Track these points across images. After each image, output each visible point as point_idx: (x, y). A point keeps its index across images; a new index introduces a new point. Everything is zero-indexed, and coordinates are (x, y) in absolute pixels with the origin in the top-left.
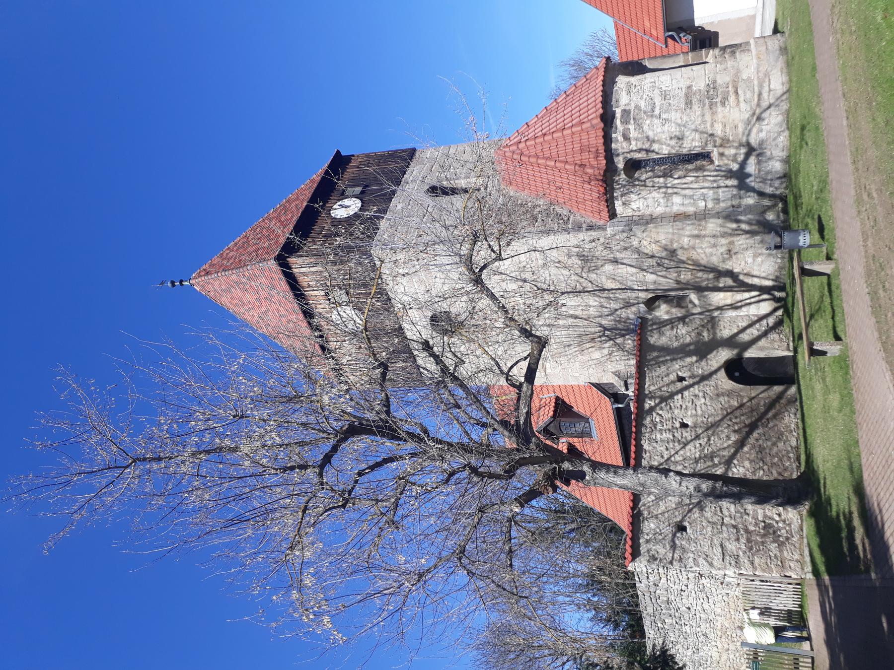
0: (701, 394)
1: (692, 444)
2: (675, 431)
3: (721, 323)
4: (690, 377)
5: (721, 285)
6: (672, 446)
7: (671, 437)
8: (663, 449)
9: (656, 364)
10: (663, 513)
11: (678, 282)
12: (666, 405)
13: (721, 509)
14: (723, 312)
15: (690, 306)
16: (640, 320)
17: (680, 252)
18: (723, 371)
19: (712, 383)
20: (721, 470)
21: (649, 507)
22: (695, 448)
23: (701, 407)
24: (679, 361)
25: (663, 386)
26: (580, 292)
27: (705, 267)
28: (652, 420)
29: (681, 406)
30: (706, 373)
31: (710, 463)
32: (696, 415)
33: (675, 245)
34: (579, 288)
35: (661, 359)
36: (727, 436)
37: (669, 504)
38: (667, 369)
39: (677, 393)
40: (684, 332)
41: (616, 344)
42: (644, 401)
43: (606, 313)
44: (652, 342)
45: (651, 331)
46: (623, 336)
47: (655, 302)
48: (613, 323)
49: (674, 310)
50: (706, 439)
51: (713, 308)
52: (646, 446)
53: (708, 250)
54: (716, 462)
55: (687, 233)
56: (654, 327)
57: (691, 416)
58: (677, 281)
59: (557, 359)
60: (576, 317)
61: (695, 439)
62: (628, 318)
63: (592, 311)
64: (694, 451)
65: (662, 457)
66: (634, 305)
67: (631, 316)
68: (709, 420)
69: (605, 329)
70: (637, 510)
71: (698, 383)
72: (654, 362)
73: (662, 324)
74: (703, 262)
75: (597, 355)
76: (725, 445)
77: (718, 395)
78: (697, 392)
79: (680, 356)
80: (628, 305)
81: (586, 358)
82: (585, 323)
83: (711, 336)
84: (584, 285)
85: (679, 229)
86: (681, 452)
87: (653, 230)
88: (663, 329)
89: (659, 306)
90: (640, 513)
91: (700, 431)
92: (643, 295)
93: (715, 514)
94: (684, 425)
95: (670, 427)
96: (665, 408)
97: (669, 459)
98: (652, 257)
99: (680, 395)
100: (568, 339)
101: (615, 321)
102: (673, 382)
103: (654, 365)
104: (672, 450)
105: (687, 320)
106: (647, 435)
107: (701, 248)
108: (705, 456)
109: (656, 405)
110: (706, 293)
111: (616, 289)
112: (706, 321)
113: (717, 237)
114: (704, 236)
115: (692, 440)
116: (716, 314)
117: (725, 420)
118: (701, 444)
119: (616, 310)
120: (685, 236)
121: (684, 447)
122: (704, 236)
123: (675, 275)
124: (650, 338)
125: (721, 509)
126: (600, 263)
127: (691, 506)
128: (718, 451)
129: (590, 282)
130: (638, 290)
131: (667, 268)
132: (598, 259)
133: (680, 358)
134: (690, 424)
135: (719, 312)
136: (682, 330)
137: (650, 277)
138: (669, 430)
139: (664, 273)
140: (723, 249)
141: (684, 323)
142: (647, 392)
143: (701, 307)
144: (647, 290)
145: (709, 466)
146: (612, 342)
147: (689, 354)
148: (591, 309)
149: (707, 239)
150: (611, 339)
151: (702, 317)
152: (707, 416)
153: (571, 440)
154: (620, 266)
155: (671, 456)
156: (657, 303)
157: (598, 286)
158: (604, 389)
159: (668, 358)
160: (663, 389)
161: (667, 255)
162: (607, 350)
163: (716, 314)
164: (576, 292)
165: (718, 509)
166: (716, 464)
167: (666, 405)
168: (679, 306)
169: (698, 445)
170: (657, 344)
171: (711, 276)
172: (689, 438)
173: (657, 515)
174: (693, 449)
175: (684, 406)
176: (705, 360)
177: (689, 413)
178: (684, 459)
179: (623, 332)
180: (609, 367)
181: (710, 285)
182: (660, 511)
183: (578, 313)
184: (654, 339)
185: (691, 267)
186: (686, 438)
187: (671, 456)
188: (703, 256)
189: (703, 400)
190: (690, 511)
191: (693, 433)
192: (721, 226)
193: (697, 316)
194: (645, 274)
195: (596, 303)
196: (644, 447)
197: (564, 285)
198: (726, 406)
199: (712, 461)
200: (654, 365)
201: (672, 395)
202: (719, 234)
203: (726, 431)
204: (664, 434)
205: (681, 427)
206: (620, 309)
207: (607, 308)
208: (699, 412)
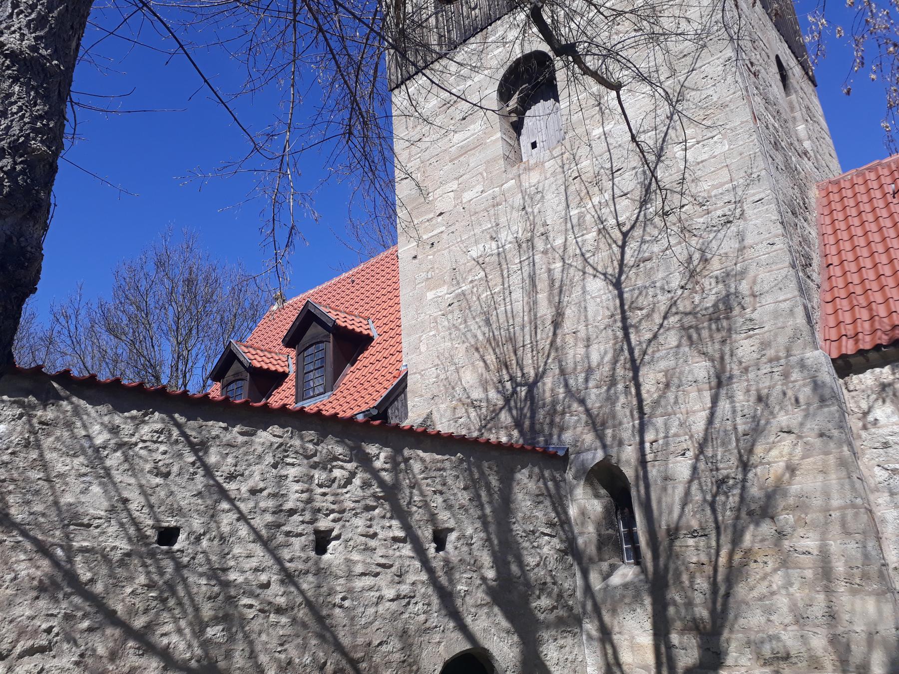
0: (405, 589)
1: (269, 561)
2: (308, 516)
3: (569, 641)
4: (447, 561)
5: (675, 638)
6: (263, 504)
7: (289, 505)
8: (255, 481)
9: (473, 480)
10: (45, 466)
11: (673, 533)
12: (375, 496)
13: (42, 650)
14: (596, 644)
15: (605, 566)
16: (561, 453)
17: (766, 528)
18: (465, 646)
19: (434, 620)
20: (182, 646)
21: (69, 425)
22: (256, 570)
23: (371, 589)
24: (482, 535)
25: (422, 494)
26: (624, 319)
27: (727, 595)
28: (336, 459)
29: (374, 536)
30: (459, 602)
31: (207, 611)
32: (350, 576)
33: (787, 518)
34: (634, 317)
35: (483, 494)
36: (290, 662)
37: (76, 485)
38: (462, 507)
39: (406, 527)
40: (546, 550)
41: (496, 413)
42: (385, 444)
43: (572, 382)
44: (518, 476)
45: (542, 477)
46: (518, 424)
47: (605, 487)
48: (548, 399)
49: (591, 528)
50: (281, 601)
51: (607, 618)
52: (264, 437)
53: (782, 602)
54: (210, 632)
55: (834, 546)
56: (550, 484)
57: (348, 560)
58: (677, 529)
59: (456, 304)
60: (557, 324)
61: (283, 569)
62: (562, 429)
63: (574, 353)
64: (247, 566)
65: (231, 477)
66: (601, 437)
67: (568, 436)
68: (337, 611)
69: (532, 387)
70: (63, 393)
71: (433, 580)
72: (476, 476)
73: (559, 503)
74: (741, 590)
75: (469, 378)
76: (263, 659)
77: (404, 634)
78: (411, 578)
79: (493, 537)
80: (597, 425)
81: (461, 355)
82: (545, 344)
83: (542, 617)
84: (644, 325)
85: (843, 524)
86: (244, 531)
87: (832, 460)
88: (547, 503)
89: (597, 496)
90: (48, 397)
91: (307, 583)
92: (629, 453)
93: (21, 633)
94: (321, 542)
95: (317, 504)
96: (369, 492)
97: (224, 494)
98: (745, 466)
99: (401, 534)
100: (502, 318)
101: (554, 403)
102: (433, 518)
103: (471, 474)
104: (251, 504)
105: (570, 559)
106: (297, 442)
107: (788, 584)
108: (231, 600)
109: (375, 473)
110: (648, 601)
111: (639, 394)
112: (571, 603)
113: (830, 626)
114: (829, 591)
115: (279, 560)
116: (590, 627)
117: (336, 656)
118: (267, 586)
119: (582, 402)
120: (823, 538)
121: (258, 538)
122: (829, 591)
123: (695, 524)
124: (525, 471)
125: (42, 650)
126: (712, 349)
127: (59, 552)
128: (246, 636)
129: (655, 336)
130: (642, 443)
131: (712, 505)
132: (723, 342)
133: (488, 540)
134: (326, 557)
135: (595, 633)
136: (549, 547)
137: (682, 468)
138: (310, 501)
139: (697, 496)
140: (789, 639)
141: (564, 552)
142: (407, 452)
143: (606, 589)
144: (643, 462)
145: (197, 609)
146: (501, 403)
147: (500, 563)
148: (581, 351)
149: (821, 597)
150: (507, 400)
151: (579, 594)
152: (347, 603)
153: (292, 375)
154: (707, 396)
155: (231, 501)
156: (603, 492)
157: (645, 353)
158: (396, 399)
159: (488, 510)
160: (415, 491)
161: (753, 499)
162: (482, 396)
163: (590, 627)
164: (623, 312)
165: (43, 641)
166: (202, 631)
167: (375, 496)
168: (602, 542)
169: (264, 578)
170: (516, 489)
171: (702, 612)
172: (286, 554)
173: (38, 446)
174: (253, 563)
175: (373, 543)
176: (488, 599)
177: (355, 556)
178: (222, 539)
179: (527, 423)
180: (443, 407)
181: (671, 610)
182: (48, 456)
183: (568, 325)
184: (526, 481)
185: (722, 560)
186: (288, 545)
187: (231, 501)
188: (762, 588)
189: (390, 593)
190: (43, 549)
191: (301, 566)
192: (871, 637)
193: (579, 581)
194: (690, 454)
195: (595, 358)
196: (260, 433)
197: (640, 283)
198: (377, 659)
199: (216, 620)
200: (471, 474)
201: (400, 514)
202: (840, 630)
203: (307, 659)
204: (297, 487)
205: (317, 532)
206: (588, 411)
207: (587, 380)
208: (359, 584)
